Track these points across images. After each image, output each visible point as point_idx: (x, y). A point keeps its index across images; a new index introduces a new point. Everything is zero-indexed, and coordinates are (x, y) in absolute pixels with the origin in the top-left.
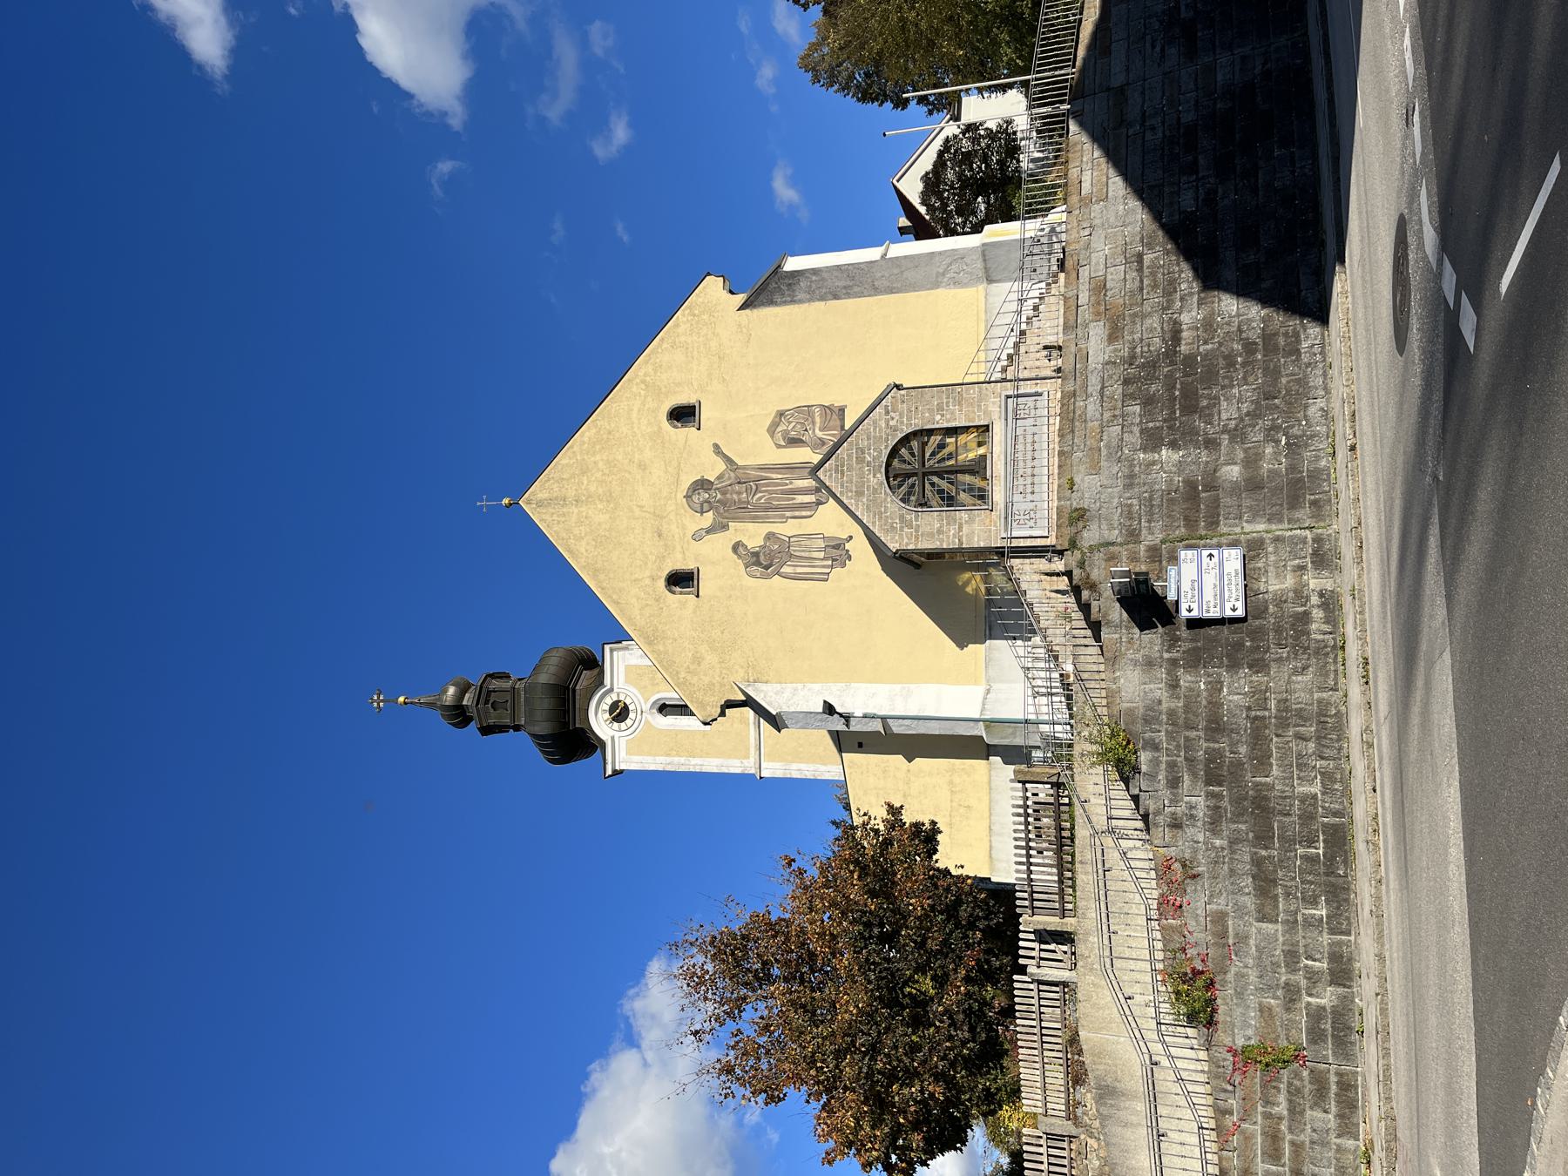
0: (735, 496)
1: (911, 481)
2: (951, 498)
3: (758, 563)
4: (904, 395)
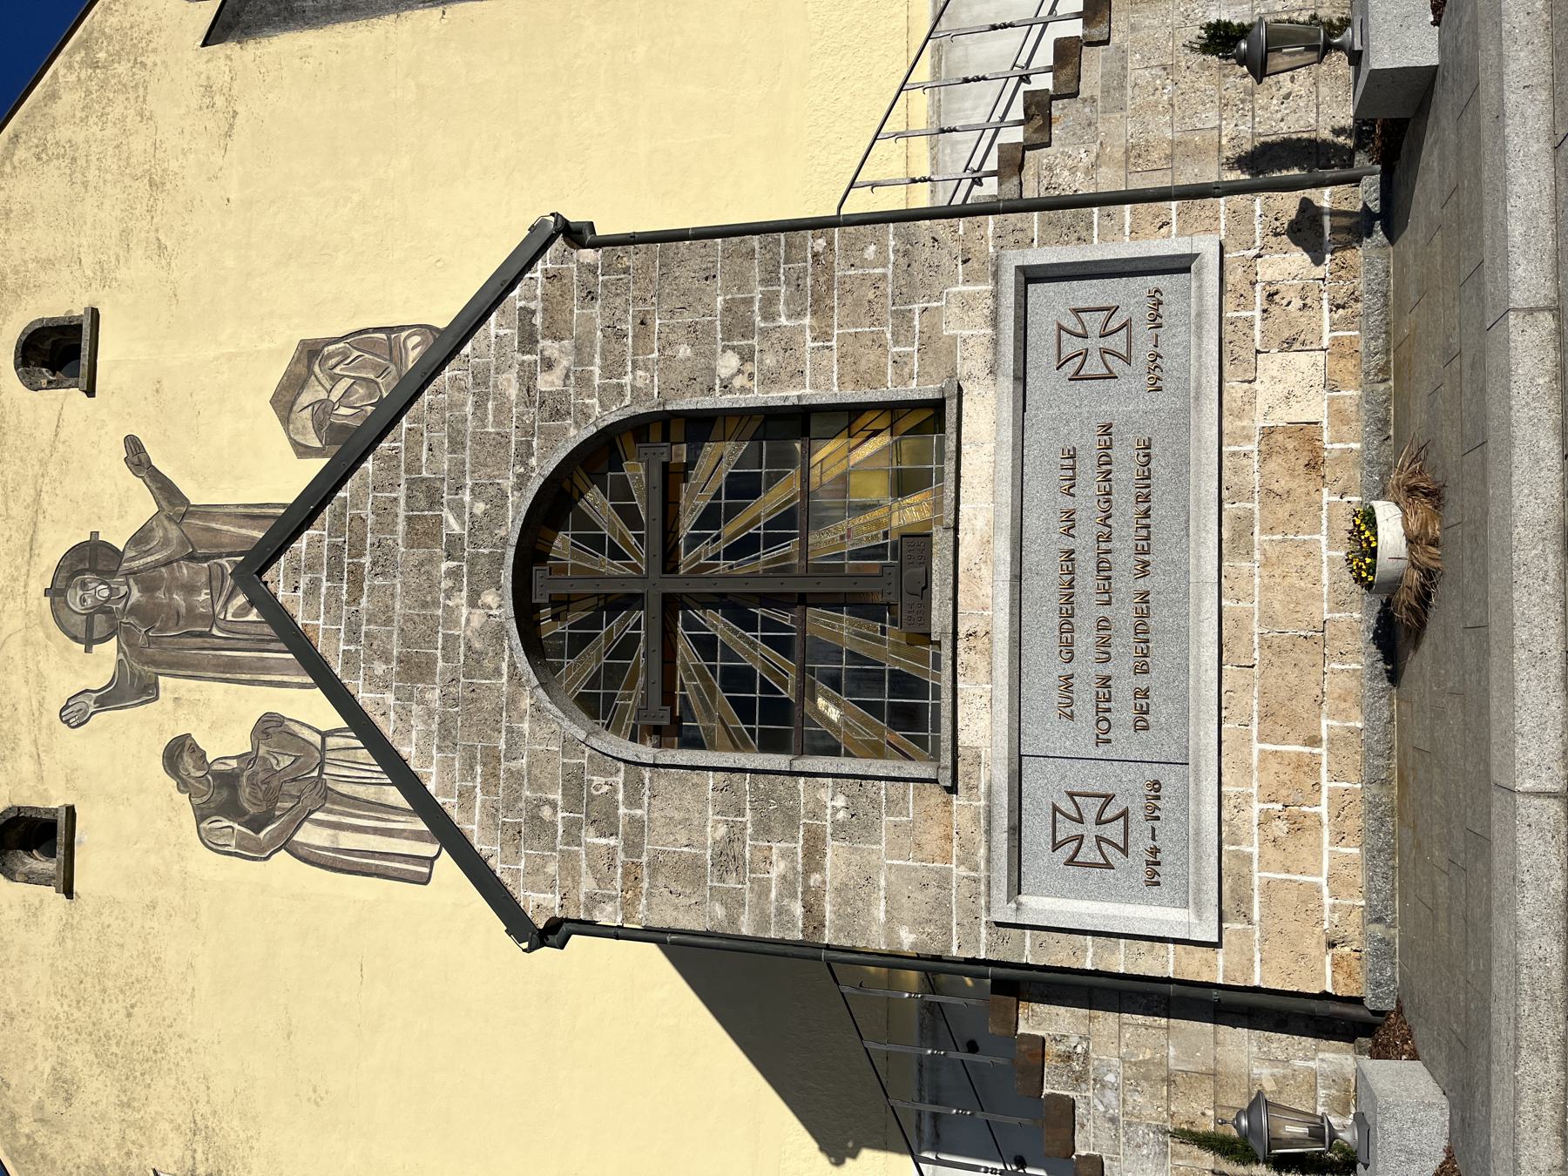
0: (178, 598)
1: (613, 629)
2: (778, 710)
3: (232, 809)
4: (592, 269)
